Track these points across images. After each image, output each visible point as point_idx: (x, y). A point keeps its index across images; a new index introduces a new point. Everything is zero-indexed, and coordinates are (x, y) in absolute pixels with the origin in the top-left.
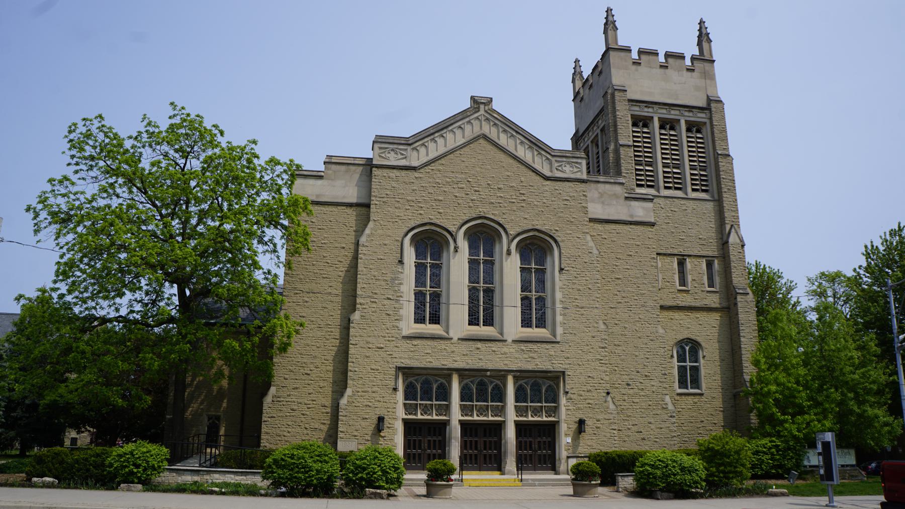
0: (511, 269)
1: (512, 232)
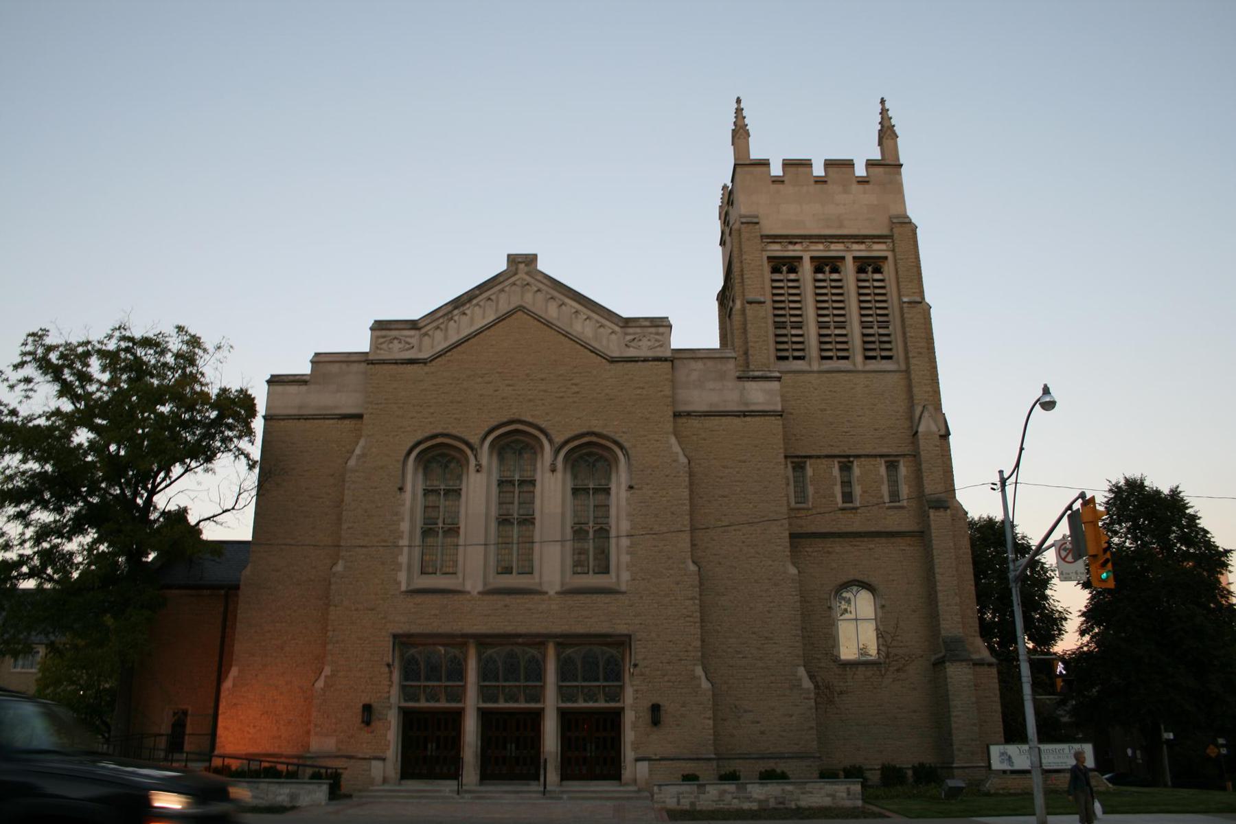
0: (552, 490)
1: (559, 440)
